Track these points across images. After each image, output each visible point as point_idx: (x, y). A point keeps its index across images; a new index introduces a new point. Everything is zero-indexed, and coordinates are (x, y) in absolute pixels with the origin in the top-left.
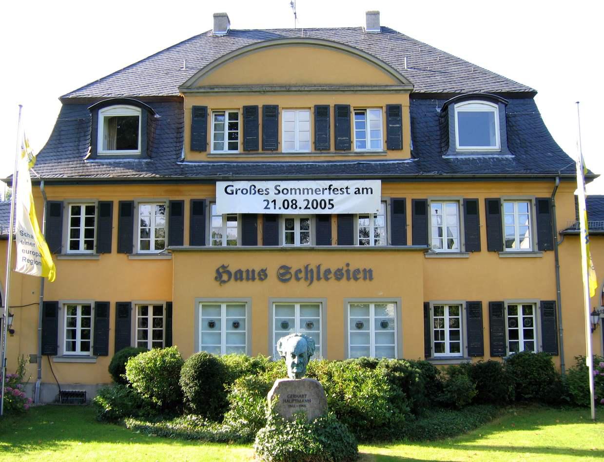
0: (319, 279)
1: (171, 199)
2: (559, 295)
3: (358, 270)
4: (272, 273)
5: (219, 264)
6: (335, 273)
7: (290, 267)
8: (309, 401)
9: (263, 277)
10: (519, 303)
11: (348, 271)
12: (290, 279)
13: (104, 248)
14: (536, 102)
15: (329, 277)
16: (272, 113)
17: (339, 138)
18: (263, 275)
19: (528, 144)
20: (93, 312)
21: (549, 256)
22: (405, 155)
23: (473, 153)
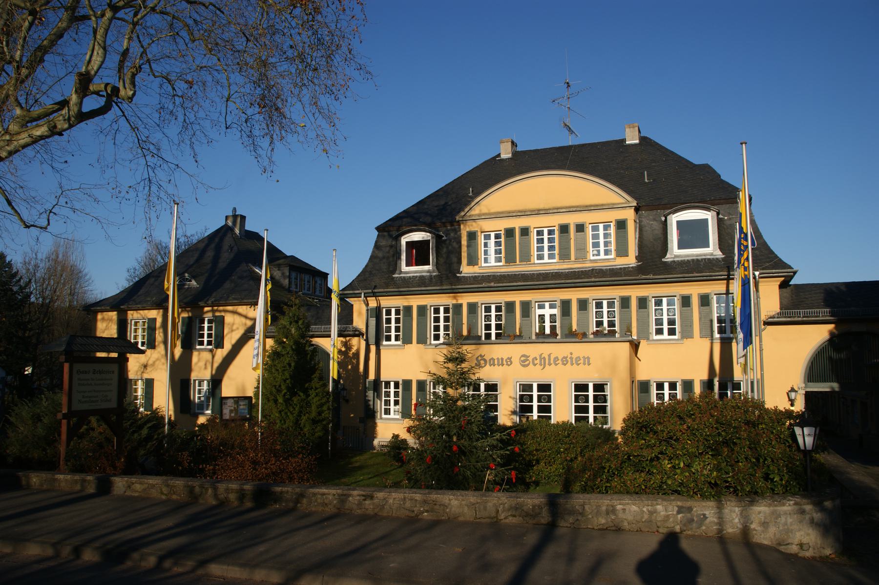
0: (550, 364)
3: (579, 357)
4: (516, 361)
6: (562, 360)
7: (528, 355)
9: (509, 363)
11: (571, 358)
13: (407, 340)
15: (557, 362)
17: (646, 180)
18: (509, 361)
20: (401, 387)
22: (631, 260)
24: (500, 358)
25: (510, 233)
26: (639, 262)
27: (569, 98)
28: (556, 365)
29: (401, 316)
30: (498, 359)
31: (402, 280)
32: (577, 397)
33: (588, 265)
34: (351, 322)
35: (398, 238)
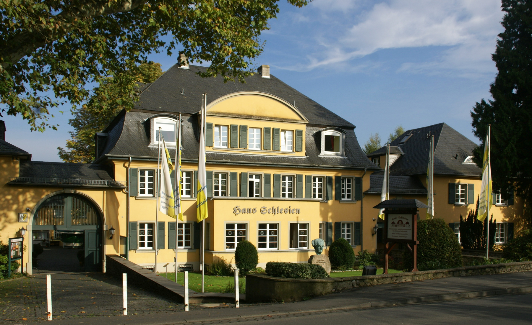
2: (362, 220)
5: (235, 206)
8: (325, 262)
14: (355, 132)
16: (244, 129)
18: (254, 211)
19: (352, 152)
21: (359, 203)
22: (302, 155)
23: (331, 155)
32: (227, 232)
33: (278, 155)
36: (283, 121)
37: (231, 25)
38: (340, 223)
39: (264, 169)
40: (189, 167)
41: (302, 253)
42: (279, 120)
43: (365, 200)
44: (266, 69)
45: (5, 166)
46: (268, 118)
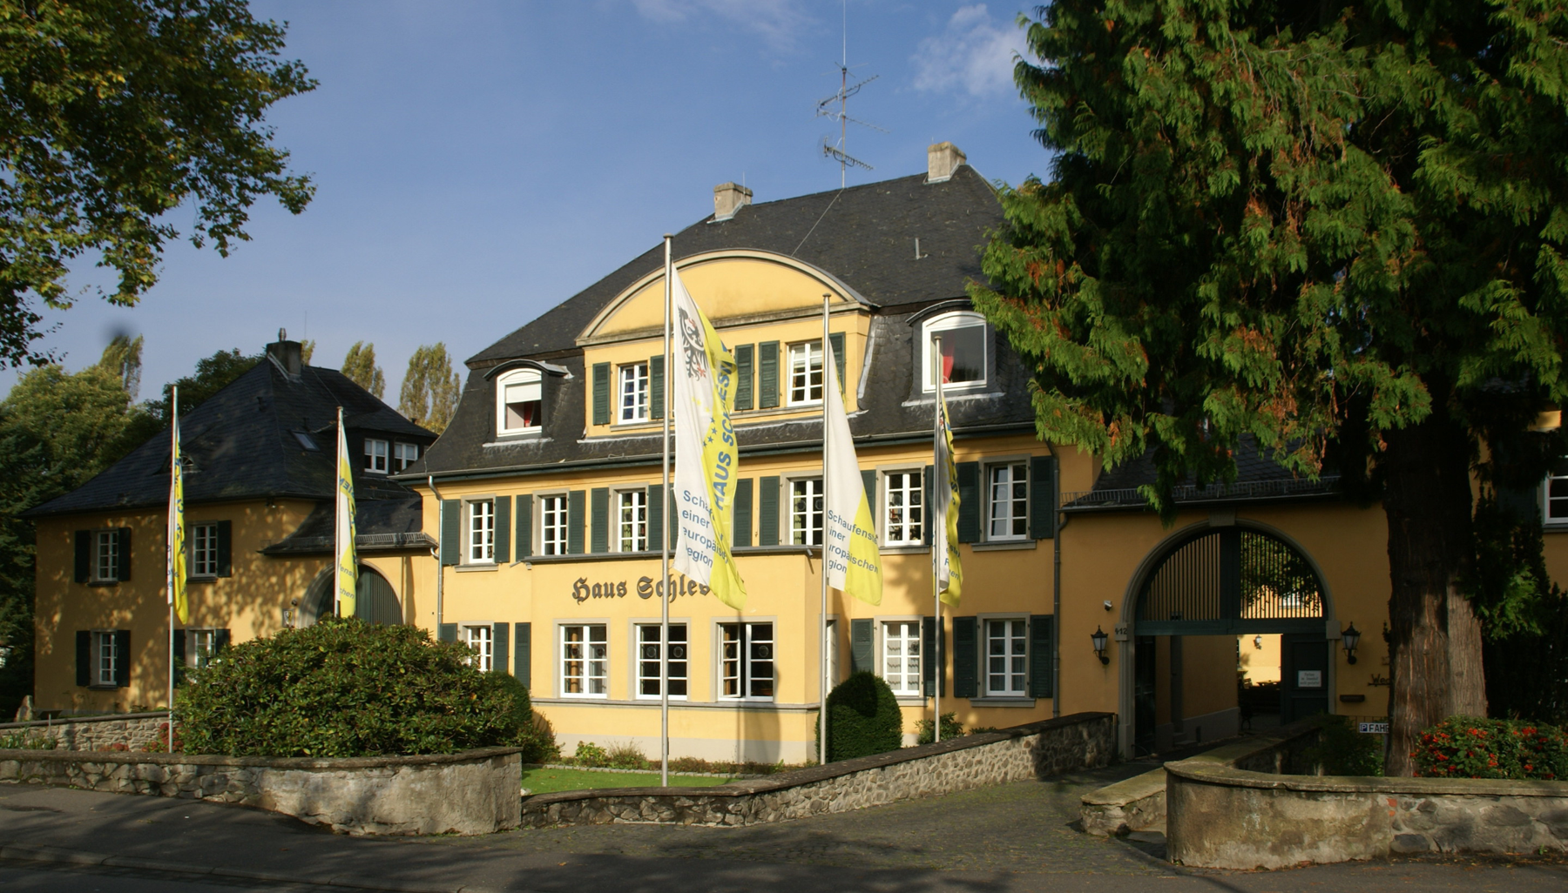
0: (682, 593)
1: (1034, 455)
2: (1058, 608)
4: (632, 588)
10: (1008, 619)
12: (651, 594)
13: (501, 555)
15: (694, 590)
21: (1046, 548)
24: (609, 583)
25: (744, 353)
26: (861, 409)
27: (845, 97)
28: (692, 594)
29: (1027, 481)
30: (606, 585)
31: (494, 452)
34: (420, 527)
35: (916, 324)
36: (784, 316)
37: (223, 111)
38: (974, 618)
39: (754, 464)
40: (557, 483)
41: (752, 715)
42: (772, 318)
43: (1071, 539)
44: (939, 154)
45: (270, 519)
46: (740, 319)
